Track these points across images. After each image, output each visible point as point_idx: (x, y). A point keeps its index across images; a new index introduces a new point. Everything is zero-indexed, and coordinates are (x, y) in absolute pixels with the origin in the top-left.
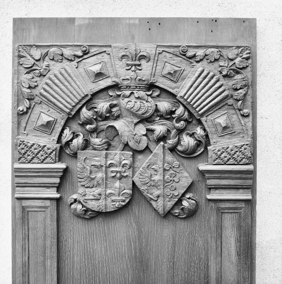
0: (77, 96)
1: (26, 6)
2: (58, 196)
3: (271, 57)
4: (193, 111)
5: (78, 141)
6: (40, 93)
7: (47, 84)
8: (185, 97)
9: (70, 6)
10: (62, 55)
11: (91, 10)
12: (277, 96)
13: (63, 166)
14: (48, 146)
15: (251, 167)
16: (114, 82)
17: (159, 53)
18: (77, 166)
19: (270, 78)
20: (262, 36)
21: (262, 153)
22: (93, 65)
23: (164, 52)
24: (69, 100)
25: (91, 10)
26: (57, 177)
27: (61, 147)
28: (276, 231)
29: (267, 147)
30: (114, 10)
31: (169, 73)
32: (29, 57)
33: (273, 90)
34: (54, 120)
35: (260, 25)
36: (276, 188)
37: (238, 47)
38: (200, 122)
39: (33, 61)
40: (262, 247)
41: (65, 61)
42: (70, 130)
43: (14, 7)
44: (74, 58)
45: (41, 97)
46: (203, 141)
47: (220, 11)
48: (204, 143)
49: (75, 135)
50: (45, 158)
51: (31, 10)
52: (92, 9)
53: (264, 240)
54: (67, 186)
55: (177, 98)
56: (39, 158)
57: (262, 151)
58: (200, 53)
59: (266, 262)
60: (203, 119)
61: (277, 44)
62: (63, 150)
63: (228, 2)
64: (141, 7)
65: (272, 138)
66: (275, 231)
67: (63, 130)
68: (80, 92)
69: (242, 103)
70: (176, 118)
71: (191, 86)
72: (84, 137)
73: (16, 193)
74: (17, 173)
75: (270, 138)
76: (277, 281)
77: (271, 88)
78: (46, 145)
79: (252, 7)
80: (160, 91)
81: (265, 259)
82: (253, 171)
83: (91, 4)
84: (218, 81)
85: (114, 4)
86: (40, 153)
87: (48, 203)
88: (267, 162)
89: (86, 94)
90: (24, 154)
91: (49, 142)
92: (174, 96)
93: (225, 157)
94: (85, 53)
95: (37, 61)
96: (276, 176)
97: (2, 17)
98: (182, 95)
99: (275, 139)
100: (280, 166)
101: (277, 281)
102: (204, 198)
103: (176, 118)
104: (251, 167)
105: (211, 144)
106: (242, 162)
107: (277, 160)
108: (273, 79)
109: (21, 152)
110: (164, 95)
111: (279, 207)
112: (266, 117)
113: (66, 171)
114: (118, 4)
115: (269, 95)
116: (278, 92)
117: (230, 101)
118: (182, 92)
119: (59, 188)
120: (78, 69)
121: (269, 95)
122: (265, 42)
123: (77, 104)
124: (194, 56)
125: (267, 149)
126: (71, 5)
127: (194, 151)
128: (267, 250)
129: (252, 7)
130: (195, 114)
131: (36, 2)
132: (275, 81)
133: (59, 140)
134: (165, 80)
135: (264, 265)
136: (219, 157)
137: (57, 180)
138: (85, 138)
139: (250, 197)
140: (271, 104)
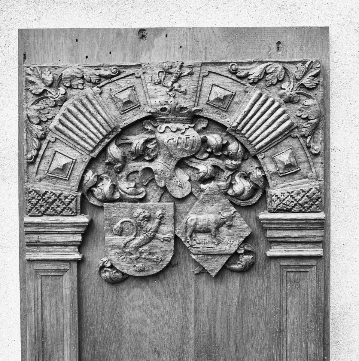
1: (35, 8)
2: (78, 256)
3: (345, 73)
4: (248, 147)
5: (105, 187)
9: (90, 9)
11: (117, 13)
12: (353, 122)
13: (83, 219)
14: (66, 193)
15: (321, 215)
16: (150, 112)
17: (204, 76)
18: (100, 219)
19: (344, 99)
20: (334, 45)
21: (335, 194)
22: (121, 90)
23: (211, 75)
24: (92, 136)
25: (117, 13)
27: (83, 196)
28: (352, 293)
30: (147, 13)
34: (73, 161)
35: (332, 33)
37: (304, 63)
38: (255, 158)
40: (334, 313)
41: (87, 85)
42: (93, 173)
45: (58, 133)
46: (260, 184)
47: (280, 15)
48: (261, 188)
50: (63, 210)
51: (41, 13)
57: (334, 192)
59: (339, 332)
60: (260, 157)
61: (353, 56)
62: (85, 199)
63: (290, 3)
64: (181, 10)
65: (346, 175)
67: (85, 171)
72: (111, 182)
73: (27, 254)
75: (344, 175)
77: (346, 112)
78: (63, 193)
79: (321, 9)
81: (337, 328)
82: (323, 220)
83: (118, 6)
84: (279, 107)
85: (146, 6)
87: (66, 266)
88: (340, 205)
89: (113, 127)
90: (36, 204)
91: (69, 189)
96: (351, 223)
97: (5, 22)
99: (350, 176)
101: (353, 356)
104: (321, 215)
105: (271, 186)
106: (311, 209)
108: (348, 101)
112: (339, 149)
114: (151, 6)
115: (343, 121)
116: (354, 117)
119: (81, 247)
120: (102, 95)
122: (337, 54)
124: (247, 75)
125: (340, 189)
126: (93, 7)
128: (340, 317)
129: (321, 9)
132: (350, 103)
133: (80, 187)
134: (212, 110)
135: (336, 336)
137: (78, 238)
138: (112, 183)
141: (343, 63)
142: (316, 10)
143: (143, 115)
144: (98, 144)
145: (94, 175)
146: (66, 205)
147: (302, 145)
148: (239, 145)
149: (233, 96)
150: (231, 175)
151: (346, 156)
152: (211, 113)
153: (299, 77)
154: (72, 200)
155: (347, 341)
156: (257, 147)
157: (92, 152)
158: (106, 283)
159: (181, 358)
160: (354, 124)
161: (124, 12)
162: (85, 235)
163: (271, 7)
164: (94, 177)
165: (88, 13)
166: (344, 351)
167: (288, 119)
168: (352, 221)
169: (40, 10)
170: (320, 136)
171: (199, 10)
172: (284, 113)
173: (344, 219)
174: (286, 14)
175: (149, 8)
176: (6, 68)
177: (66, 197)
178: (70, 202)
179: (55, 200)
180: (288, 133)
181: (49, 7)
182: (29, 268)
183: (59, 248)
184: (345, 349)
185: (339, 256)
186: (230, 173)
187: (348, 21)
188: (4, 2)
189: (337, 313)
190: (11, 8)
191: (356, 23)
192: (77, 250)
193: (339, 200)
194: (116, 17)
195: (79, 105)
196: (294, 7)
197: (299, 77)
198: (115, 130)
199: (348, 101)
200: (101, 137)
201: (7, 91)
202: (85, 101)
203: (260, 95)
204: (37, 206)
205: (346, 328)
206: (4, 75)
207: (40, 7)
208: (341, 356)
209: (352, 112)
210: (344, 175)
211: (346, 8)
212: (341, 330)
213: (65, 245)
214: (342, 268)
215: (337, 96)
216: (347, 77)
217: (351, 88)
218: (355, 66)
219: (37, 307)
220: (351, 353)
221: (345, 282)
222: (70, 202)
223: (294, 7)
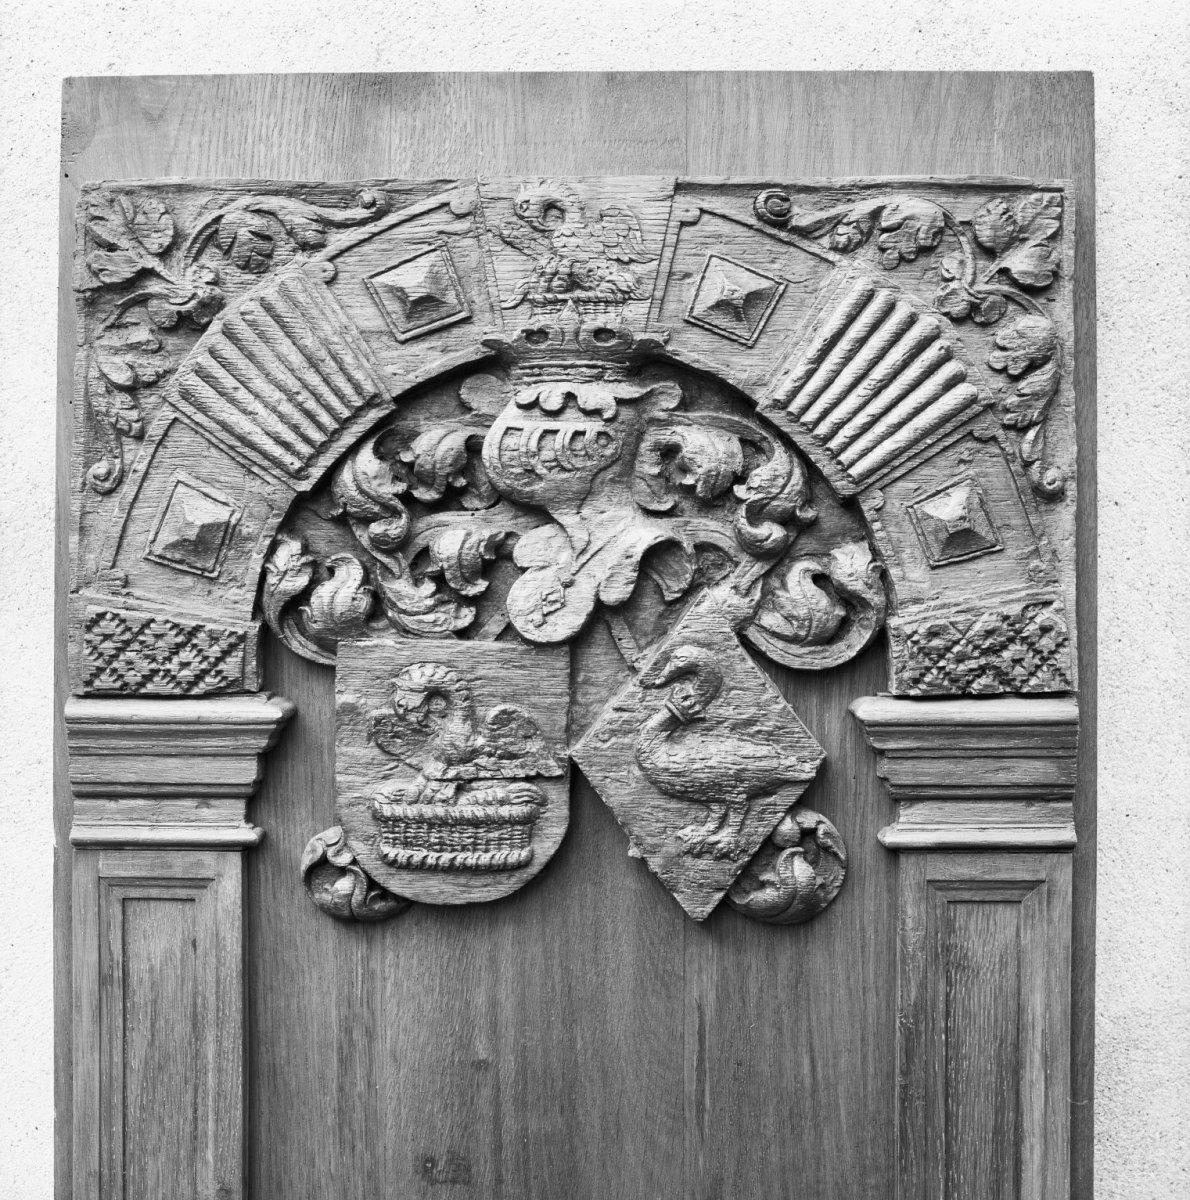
0: (325, 418)
2: (249, 834)
4: (827, 468)
5: (342, 590)
7: (200, 372)
12: (1161, 409)
13: (267, 710)
15: (1065, 710)
17: (683, 224)
19: (1131, 333)
28: (1154, 976)
33: (1142, 385)
36: (1156, 794)
49: (320, 572)
53: (1106, 1014)
55: (758, 409)
56: (174, 677)
59: (1112, 1105)
62: (278, 642)
65: (1139, 585)
66: (1149, 975)
68: (348, 390)
69: (1037, 437)
74: (77, 736)
75: (1131, 586)
76: (1158, 1183)
81: (1106, 1090)
91: (225, 609)
92: (739, 401)
93: (1017, 661)
98: (780, 395)
100: (1172, 701)
101: (1158, 1183)
102: (869, 845)
104: (1065, 710)
108: (1145, 338)
112: (1116, 499)
113: (286, 730)
115: (1127, 405)
117: (986, 426)
119: (254, 800)
121: (1127, 405)
126: (300, 24)
128: (1116, 1055)
132: (1150, 345)
136: (1044, 659)
137: (246, 772)
139: (1068, 835)
140: (1136, 445)
141: (1129, 214)
143: (469, 353)
145: (304, 560)
148: (791, 462)
151: (1138, 523)
152: (694, 350)
153: (996, 218)
154: (232, 647)
155: (1138, 1136)
156: (855, 471)
157: (298, 475)
158: (330, 922)
159: (997, 1192)
160: (1165, 418)
162: (269, 759)
164: (303, 565)
166: (1129, 1167)
168: (1158, 738)
170: (1063, 430)
172: (947, 357)
173: (1131, 729)
177: (214, 638)
178: (226, 653)
179: (179, 647)
180: (961, 426)
182: (83, 875)
184: (1131, 1163)
185: (1114, 855)
186: (758, 568)
187: (1147, 77)
191: (1171, 84)
193: (1113, 668)
194: (378, 60)
197: (996, 218)
203: (868, 297)
204: (115, 665)
205: (1136, 1090)
208: (1119, 1183)
209: (1158, 375)
210: (1131, 586)
213: (206, 795)
214: (1122, 894)
215: (1109, 324)
217: (1153, 297)
218: (1170, 224)
219: (361, 1087)
222: (226, 653)
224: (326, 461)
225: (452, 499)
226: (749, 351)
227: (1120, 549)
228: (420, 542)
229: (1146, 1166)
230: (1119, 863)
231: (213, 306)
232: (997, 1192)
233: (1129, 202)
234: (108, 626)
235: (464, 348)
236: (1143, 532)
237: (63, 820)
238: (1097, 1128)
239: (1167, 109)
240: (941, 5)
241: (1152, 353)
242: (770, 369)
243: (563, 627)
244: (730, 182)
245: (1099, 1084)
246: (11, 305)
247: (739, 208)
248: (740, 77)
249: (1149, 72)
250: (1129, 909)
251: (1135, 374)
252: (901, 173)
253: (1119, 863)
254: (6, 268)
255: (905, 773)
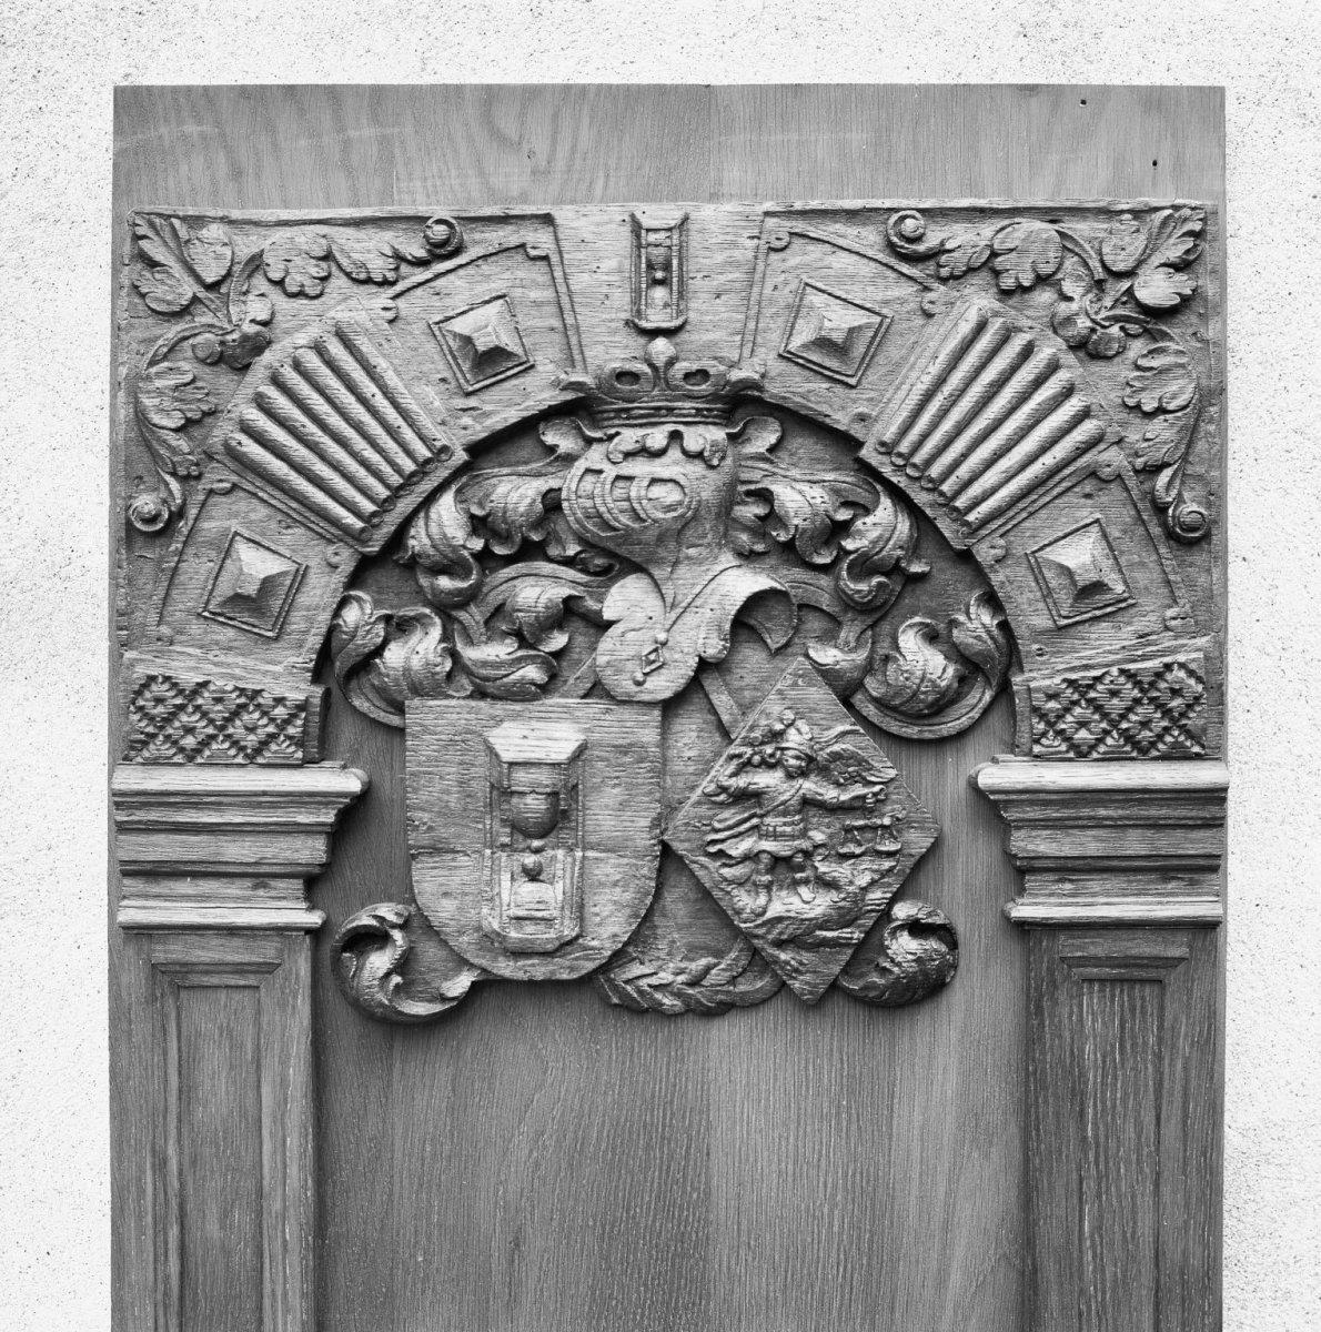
1: (125, 35)
2: (314, 919)
3: (1264, 274)
6: (226, 445)
8: (904, 447)
9: (328, 37)
10: (328, 257)
12: (1294, 454)
26: (320, 833)
28: (1288, 1083)
29: (1244, 691)
31: (823, 343)
32: (177, 269)
33: (1273, 428)
34: (298, 570)
39: (189, 289)
43: (69, 42)
44: (396, 269)
51: (148, 53)
52: (433, 52)
53: (1233, 1125)
54: (353, 873)
55: (864, 453)
58: (964, 239)
59: (1241, 1226)
65: (1270, 649)
66: (1282, 1082)
70: (851, 557)
71: (928, 396)
80: (782, 425)
85: (535, 28)
86: (223, 724)
92: (846, 444)
94: (442, 250)
95: (213, 287)
103: (851, 557)
107: (1295, 751)
109: (148, 719)
110: (803, 445)
111: (1304, 970)
112: (1244, 554)
118: (889, 424)
123: (410, 481)
126: (337, 31)
127: (943, 703)
130: (946, 527)
131: (171, 19)
141: (1257, 238)
142: (1159, 42)
144: (397, 493)
146: (277, 726)
147: (1136, 507)
149: (881, 335)
150: (872, 627)
151: (1269, 581)
161: (454, 50)
163: (992, 32)
165: (319, 54)
166: (1259, 1295)
167: (1085, 414)
168: (1291, 819)
169: (144, 42)
171: (727, 41)
172: (1068, 392)
174: (1047, 60)
175: (542, 34)
176: (16, 254)
181: (178, 31)
183: (235, 889)
187: (1278, 86)
188: (13, 14)
189: (1235, 1155)
190: (36, 32)
192: (300, 894)
193: (1241, 742)
194: (423, 70)
195: (312, 361)
196: (1076, 34)
198: (444, 457)
199: (1276, 378)
200: (383, 493)
201: (21, 340)
202: (336, 349)
205: (1267, 1210)
206: (12, 281)
207: (143, 30)
211: (1268, 37)
212: (1250, 1219)
216: (1273, 291)
217: (1285, 330)
218: (1303, 249)
220: (1286, 1304)
221: (1262, 1044)
223: (1076, 34)
224: (405, 505)
225: (529, 551)
226: (853, 394)
227: (1248, 610)
228: (494, 599)
229: (1278, 1294)
230: (1248, 958)
231: (257, 345)
232: (1081, 1329)
233: (1258, 224)
234: (159, 689)
235: (537, 392)
236: (1274, 591)
237: (116, 898)
238: (1226, 1252)
239: (1299, 121)
240: (1048, 6)
241: (1284, 394)
242: (883, 409)
243: (663, 685)
244: (807, 208)
245: (1228, 1202)
246: (15, 342)
247: (869, 237)
248: (783, 85)
249: (1281, 80)
250: (1260, 1010)
251: (1264, 415)
252: (357, 205)
253: (1248, 958)
254: (10, 302)
255: (1042, 844)
